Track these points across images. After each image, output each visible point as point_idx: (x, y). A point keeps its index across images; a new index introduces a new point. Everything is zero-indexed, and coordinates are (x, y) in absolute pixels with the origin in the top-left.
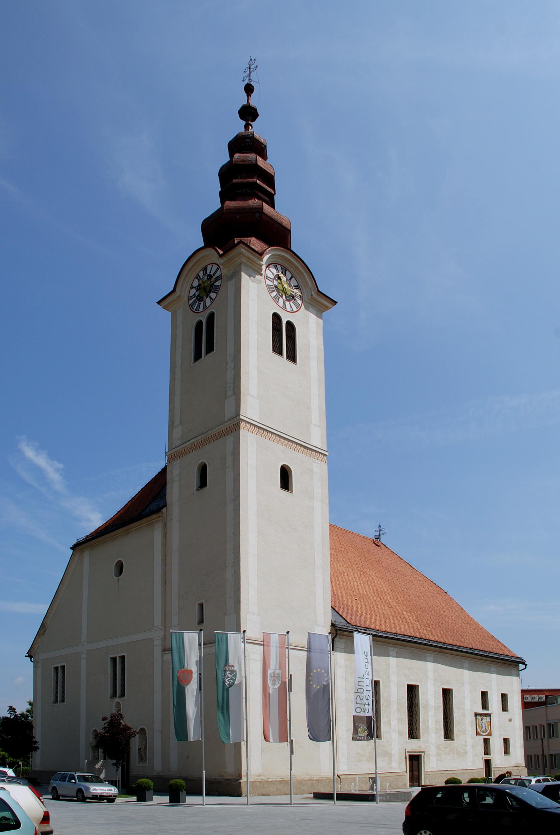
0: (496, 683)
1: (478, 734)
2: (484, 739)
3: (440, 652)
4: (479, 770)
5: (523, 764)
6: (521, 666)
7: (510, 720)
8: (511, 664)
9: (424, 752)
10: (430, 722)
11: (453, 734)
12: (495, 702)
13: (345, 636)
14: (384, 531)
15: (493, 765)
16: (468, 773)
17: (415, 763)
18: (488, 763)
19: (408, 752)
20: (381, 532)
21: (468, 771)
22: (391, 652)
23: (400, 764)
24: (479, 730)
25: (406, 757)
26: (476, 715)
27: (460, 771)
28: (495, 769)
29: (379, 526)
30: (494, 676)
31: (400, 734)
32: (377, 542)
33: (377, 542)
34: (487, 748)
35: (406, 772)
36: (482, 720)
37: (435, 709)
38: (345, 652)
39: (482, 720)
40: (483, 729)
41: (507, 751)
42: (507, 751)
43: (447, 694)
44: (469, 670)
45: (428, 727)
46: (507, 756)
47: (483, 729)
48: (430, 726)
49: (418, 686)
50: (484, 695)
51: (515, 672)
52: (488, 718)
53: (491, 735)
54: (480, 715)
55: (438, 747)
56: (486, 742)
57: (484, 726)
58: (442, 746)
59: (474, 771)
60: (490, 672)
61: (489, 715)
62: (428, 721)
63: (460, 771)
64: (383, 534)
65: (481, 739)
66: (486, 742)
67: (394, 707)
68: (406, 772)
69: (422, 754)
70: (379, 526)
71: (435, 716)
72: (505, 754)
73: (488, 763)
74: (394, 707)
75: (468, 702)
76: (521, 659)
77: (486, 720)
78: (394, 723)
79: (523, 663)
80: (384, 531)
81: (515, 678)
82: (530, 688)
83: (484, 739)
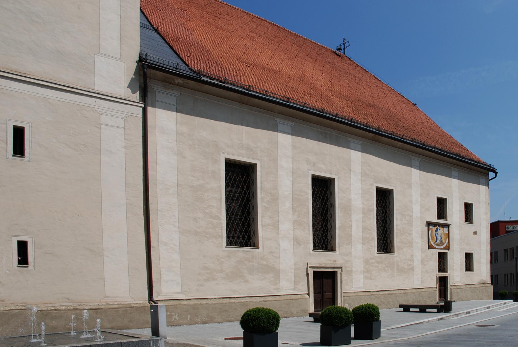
0: (458, 190)
1: (430, 247)
2: (439, 253)
3: (373, 140)
4: (431, 290)
5: (489, 280)
6: (491, 175)
7: (475, 233)
8: (478, 170)
9: (341, 268)
10: (354, 228)
11: (393, 246)
12: (455, 213)
13: (178, 85)
14: (348, 44)
15: (450, 283)
16: (414, 293)
17: (327, 282)
18: (443, 282)
19: (310, 267)
20: (346, 45)
21: (414, 291)
22: (280, 126)
23: (296, 283)
24: (432, 243)
25: (308, 274)
26: (429, 224)
27: (402, 291)
28: (451, 287)
29: (344, 40)
30: (455, 182)
31: (297, 242)
32: (339, 53)
33: (339, 53)
34: (470, 264)
35: (308, 294)
36: (437, 231)
37: (363, 213)
38: (178, 111)
39: (437, 231)
40: (439, 241)
41: (469, 267)
42: (469, 267)
43: (384, 197)
44: (420, 170)
45: (350, 236)
46: (469, 273)
47: (439, 241)
48: (353, 233)
49: (334, 179)
50: (441, 203)
51: (483, 180)
52: (446, 230)
53: (449, 249)
54: (435, 224)
55: (367, 262)
56: (442, 258)
57: (439, 238)
58: (373, 261)
59: (423, 290)
60: (451, 176)
61: (448, 226)
62: (350, 227)
63: (402, 291)
64: (347, 47)
65: (434, 254)
66: (442, 258)
67: (286, 205)
68: (308, 294)
69: (339, 271)
70: (344, 40)
71: (363, 222)
72: (466, 270)
73: (443, 282)
74: (286, 205)
75: (416, 209)
76: (490, 167)
77: (442, 231)
78: (285, 227)
79: (494, 171)
80: (348, 44)
81: (483, 188)
82: (512, 219)
83: (439, 253)
